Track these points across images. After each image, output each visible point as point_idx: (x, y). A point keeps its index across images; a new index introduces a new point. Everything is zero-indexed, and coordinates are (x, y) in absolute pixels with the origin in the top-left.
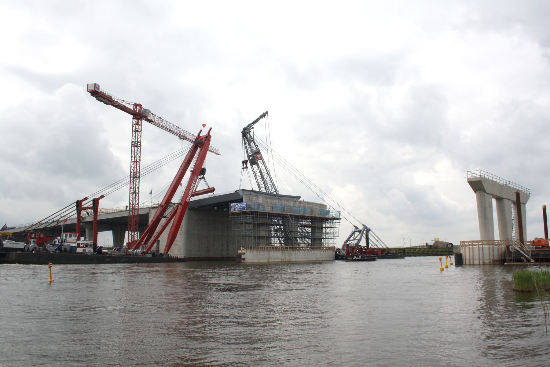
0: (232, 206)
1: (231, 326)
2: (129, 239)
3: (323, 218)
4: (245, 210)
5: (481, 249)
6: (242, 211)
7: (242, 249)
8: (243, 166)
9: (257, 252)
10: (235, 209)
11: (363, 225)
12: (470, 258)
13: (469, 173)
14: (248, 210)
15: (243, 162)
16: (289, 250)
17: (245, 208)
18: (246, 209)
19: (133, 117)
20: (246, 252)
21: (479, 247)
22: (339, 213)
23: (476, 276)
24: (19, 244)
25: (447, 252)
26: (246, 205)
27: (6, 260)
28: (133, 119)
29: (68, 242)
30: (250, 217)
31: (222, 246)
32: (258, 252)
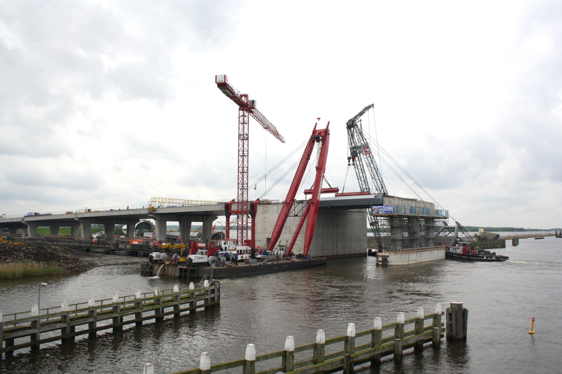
0: (375, 208)
2: (239, 237)
4: (392, 213)
8: (349, 162)
10: (378, 212)
11: (457, 223)
15: (349, 159)
17: (392, 212)
18: (393, 212)
19: (239, 108)
22: (447, 212)
26: (393, 209)
27: (196, 275)
28: (240, 109)
29: (230, 250)
31: (333, 244)
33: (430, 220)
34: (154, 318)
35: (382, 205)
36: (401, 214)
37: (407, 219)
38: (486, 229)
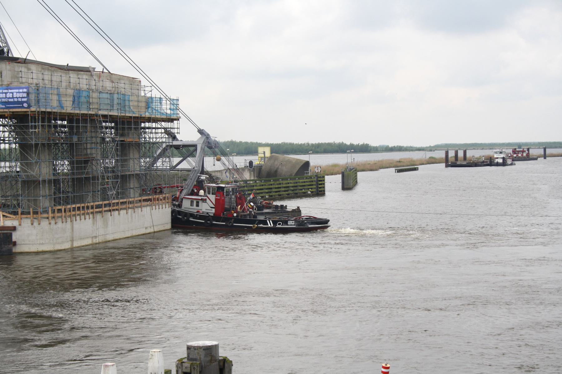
1: (499, 238)
4: (23, 107)
6: (11, 110)
9: (50, 224)
11: (201, 132)
16: (105, 211)
17: (22, 103)
18: (25, 105)
20: (20, 225)
24: (206, 209)
26: (25, 95)
32: (53, 222)
38: (277, 149)
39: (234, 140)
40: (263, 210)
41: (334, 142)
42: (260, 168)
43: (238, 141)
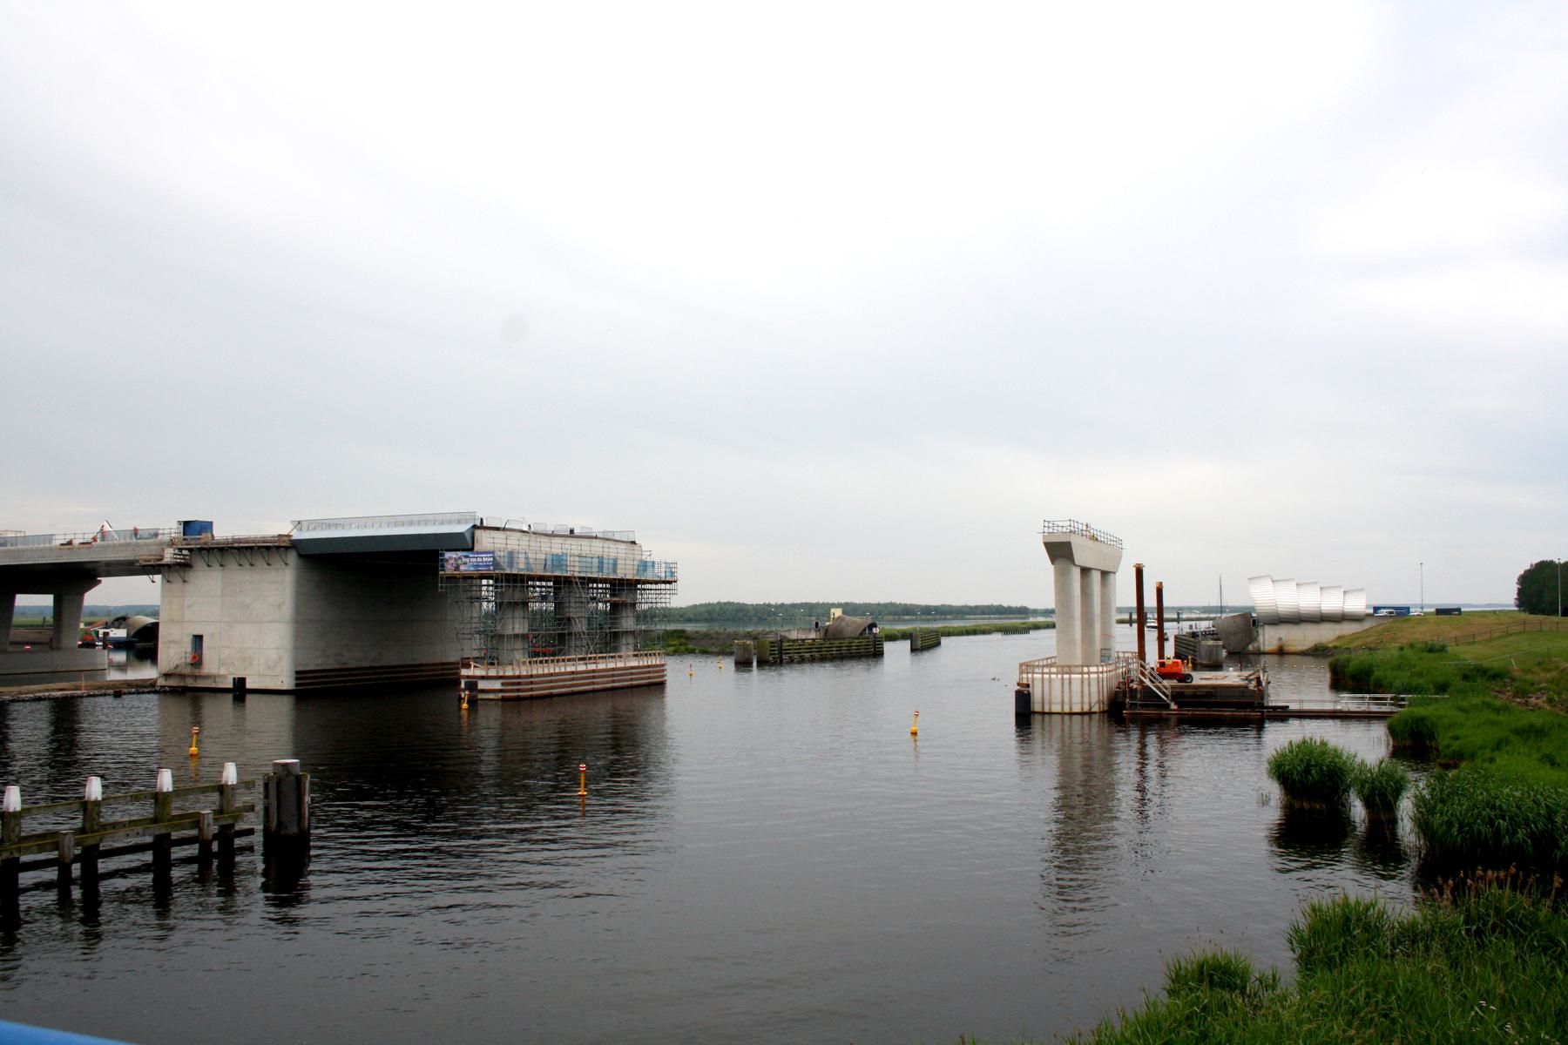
3: (589, 578)
4: (489, 570)
5: (1066, 683)
7: (475, 667)
12: (1043, 699)
13: (1046, 524)
14: (497, 572)
17: (489, 566)
18: (492, 568)
21: (1062, 678)
23: (1175, 768)
25: (774, 647)
26: (492, 559)
30: (502, 587)
33: (623, 589)
34: (175, 840)
35: (471, 549)
36: (515, 572)
37: (552, 584)
39: (893, 602)
40: (1028, 618)
41: (1532, 565)
42: (827, 630)
43: (898, 603)
